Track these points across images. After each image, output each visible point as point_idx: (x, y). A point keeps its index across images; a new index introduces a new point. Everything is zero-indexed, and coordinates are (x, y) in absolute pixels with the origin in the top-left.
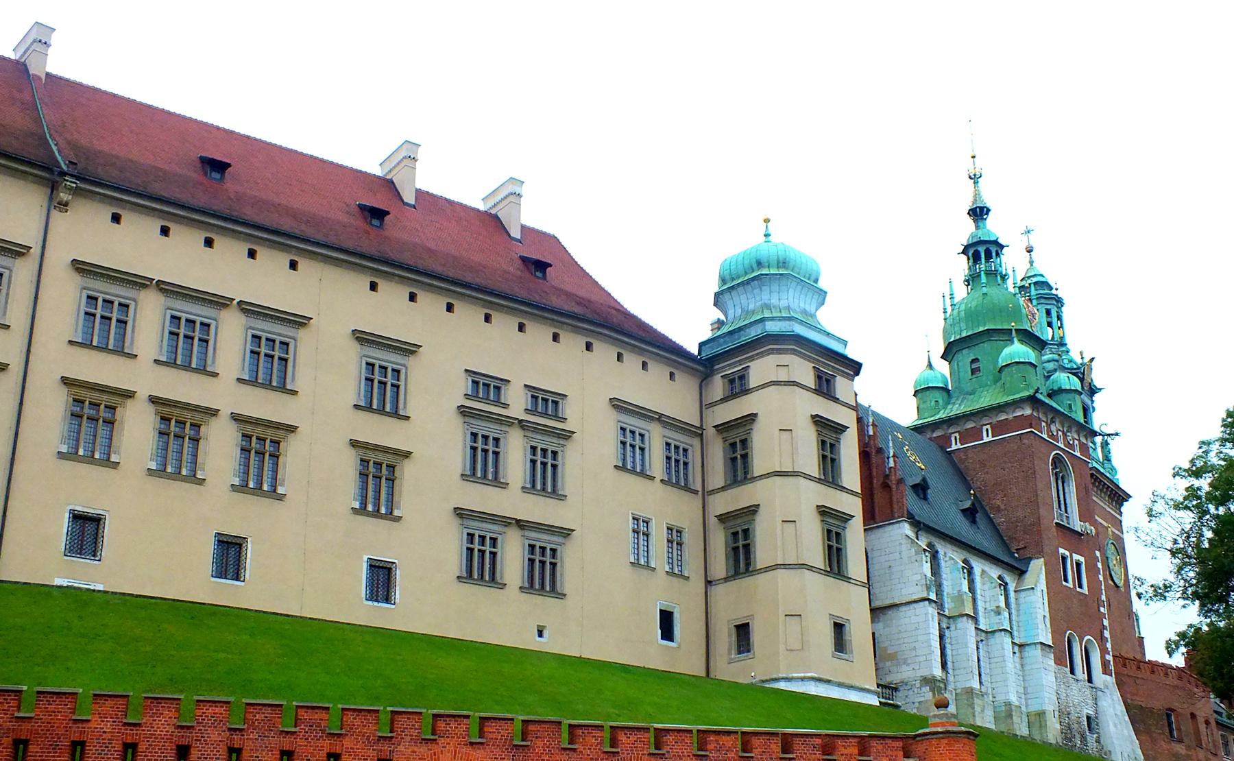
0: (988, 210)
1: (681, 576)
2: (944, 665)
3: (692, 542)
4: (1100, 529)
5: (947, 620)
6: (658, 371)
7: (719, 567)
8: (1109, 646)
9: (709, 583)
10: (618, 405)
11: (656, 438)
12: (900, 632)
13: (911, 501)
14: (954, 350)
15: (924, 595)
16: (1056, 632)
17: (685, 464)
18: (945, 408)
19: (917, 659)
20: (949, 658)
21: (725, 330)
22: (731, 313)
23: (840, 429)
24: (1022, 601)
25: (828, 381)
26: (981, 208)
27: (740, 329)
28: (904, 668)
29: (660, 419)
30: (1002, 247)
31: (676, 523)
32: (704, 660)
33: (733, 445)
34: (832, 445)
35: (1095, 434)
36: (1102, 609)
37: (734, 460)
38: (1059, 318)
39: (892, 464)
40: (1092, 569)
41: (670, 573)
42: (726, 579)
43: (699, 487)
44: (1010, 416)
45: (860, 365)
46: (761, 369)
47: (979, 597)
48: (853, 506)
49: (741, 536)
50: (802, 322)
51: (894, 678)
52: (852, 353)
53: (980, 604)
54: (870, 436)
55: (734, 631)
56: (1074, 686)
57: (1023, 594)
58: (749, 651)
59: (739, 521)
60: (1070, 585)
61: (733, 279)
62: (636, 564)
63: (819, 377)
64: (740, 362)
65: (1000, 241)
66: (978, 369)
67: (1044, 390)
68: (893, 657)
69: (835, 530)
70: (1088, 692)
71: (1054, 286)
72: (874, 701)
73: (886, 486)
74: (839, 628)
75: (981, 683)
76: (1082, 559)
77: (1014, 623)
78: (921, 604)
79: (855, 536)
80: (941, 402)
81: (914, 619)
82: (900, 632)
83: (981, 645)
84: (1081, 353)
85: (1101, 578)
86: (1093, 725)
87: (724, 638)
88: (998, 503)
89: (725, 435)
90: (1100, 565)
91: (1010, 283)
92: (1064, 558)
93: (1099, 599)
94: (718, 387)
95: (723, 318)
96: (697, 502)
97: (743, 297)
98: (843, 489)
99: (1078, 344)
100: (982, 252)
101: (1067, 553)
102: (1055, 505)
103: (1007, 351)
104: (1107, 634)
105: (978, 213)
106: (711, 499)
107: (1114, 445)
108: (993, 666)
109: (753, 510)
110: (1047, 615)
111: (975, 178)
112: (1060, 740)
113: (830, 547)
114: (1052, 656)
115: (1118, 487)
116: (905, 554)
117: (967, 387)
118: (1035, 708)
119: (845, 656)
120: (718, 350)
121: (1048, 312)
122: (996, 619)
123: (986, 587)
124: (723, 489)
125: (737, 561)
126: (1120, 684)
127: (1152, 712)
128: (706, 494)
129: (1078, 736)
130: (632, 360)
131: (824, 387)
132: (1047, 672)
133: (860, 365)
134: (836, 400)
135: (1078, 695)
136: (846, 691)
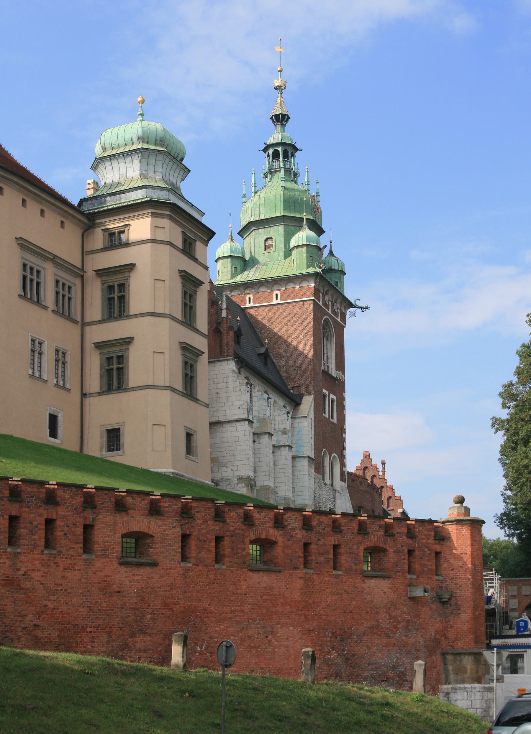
0: (289, 118)
1: (64, 388)
3: (73, 359)
6: (52, 219)
7: (94, 382)
9: (84, 395)
10: (24, 245)
11: (49, 275)
12: (223, 442)
15: (245, 416)
16: (318, 449)
17: (69, 299)
24: (296, 425)
25: (190, 244)
26: (284, 116)
28: (224, 469)
29: (54, 259)
30: (296, 150)
31: (61, 346)
34: (191, 296)
37: (111, 300)
41: (57, 385)
42: (100, 394)
43: (79, 319)
48: (201, 344)
49: (115, 360)
52: (205, 221)
57: (297, 421)
58: (118, 449)
59: (114, 349)
60: (327, 415)
61: (113, 148)
62: (33, 376)
63: (185, 240)
69: (190, 362)
74: (189, 436)
76: (335, 398)
78: (242, 423)
82: (223, 442)
88: (281, 351)
89: (104, 278)
97: (122, 165)
98: (197, 331)
106: (88, 329)
108: (278, 471)
109: (128, 341)
110: (313, 436)
113: (186, 375)
114: (313, 466)
119: (193, 458)
124: (100, 322)
128: (84, 324)
130: (34, 207)
133: (214, 234)
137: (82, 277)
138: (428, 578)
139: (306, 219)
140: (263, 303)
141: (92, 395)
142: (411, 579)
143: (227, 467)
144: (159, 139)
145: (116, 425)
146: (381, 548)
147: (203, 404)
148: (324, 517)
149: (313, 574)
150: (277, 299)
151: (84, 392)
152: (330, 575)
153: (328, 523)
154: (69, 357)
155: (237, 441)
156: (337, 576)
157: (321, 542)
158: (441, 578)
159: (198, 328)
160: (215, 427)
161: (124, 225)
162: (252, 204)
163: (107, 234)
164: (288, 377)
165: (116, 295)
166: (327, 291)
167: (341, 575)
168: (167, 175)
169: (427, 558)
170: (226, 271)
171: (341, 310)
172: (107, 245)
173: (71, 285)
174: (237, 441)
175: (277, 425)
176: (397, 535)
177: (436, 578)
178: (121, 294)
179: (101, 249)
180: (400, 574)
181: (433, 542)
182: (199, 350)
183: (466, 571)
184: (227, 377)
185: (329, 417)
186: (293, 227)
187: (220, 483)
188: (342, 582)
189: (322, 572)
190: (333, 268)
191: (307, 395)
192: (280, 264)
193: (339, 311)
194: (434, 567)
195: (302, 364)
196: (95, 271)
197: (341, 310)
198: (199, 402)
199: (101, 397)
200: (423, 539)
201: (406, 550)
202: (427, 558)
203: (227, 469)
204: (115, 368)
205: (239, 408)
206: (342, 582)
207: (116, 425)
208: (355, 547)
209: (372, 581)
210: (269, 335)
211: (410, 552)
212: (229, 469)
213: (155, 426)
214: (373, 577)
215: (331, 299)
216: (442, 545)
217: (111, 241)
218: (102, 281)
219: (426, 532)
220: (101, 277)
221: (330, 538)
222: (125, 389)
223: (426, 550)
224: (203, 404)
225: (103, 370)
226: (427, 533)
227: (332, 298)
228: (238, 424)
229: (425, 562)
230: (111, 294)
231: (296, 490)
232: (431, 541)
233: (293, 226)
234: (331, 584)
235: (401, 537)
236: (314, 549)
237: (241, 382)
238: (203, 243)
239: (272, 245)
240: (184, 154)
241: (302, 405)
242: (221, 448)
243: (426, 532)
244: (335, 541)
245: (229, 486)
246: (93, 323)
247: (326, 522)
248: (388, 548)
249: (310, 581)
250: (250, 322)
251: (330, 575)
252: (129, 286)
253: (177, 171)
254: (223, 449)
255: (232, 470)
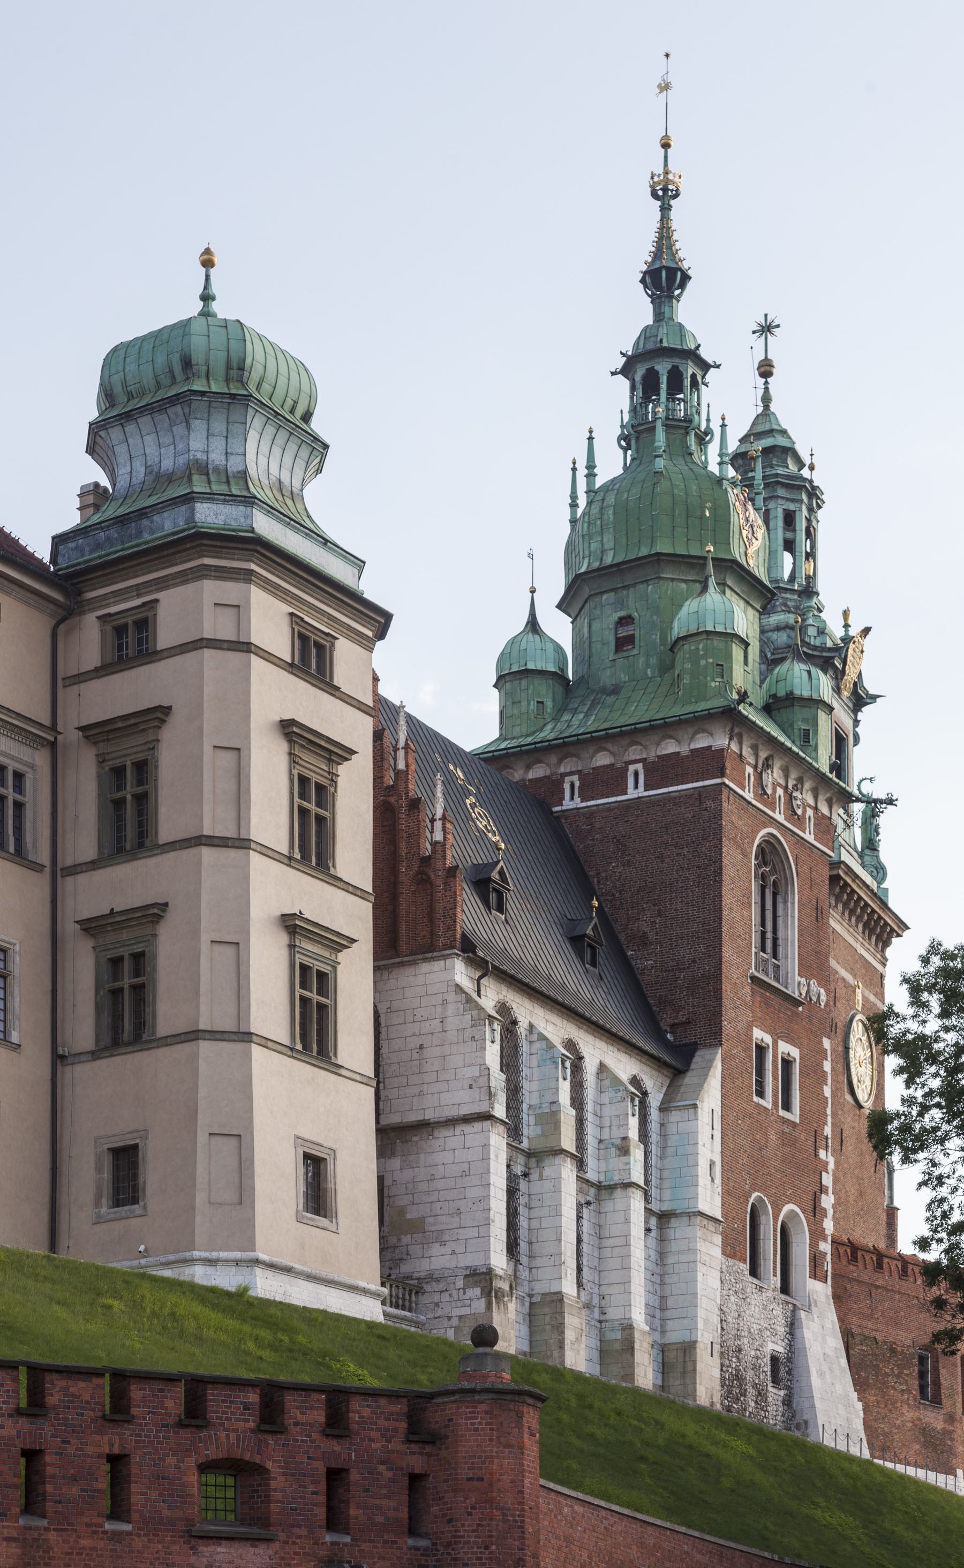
2: (512, 1248)
4: (841, 992)
5: (531, 1158)
7: (82, 1030)
8: (829, 1225)
9: (58, 1059)
12: (432, 1179)
13: (470, 913)
14: (586, 591)
18: (556, 719)
19: (463, 1234)
20: (523, 1234)
21: (110, 511)
22: (123, 472)
23: (336, 753)
24: (672, 1129)
27: (142, 513)
28: (436, 1249)
32: (45, 1215)
33: (119, 772)
35: (846, 798)
36: (822, 1154)
38: (810, 534)
39: (438, 836)
40: (813, 1073)
42: (95, 1055)
44: (684, 749)
45: (388, 617)
46: (185, 608)
47: (590, 1116)
48: (353, 917)
49: (127, 966)
50: (271, 510)
51: (419, 1266)
52: (371, 588)
53: (591, 1131)
54: (398, 773)
55: (107, 1161)
56: (756, 1300)
58: (135, 1201)
59: (125, 935)
60: (767, 1103)
64: (138, 590)
65: (704, 353)
66: (630, 640)
67: (757, 696)
68: (417, 1226)
69: (318, 966)
70: (778, 1311)
71: (807, 460)
72: (371, 1310)
73: (423, 880)
75: (580, 1285)
76: (795, 1053)
77: (653, 1171)
79: (355, 977)
80: (549, 704)
81: (461, 1155)
82: (432, 1179)
83: (586, 1212)
84: (846, 614)
85: (827, 1091)
86: (782, 1372)
87: (86, 1176)
90: (827, 1066)
91: (713, 449)
92: (761, 1050)
93: (817, 1134)
94: (89, 641)
95: (105, 482)
96: (39, 885)
98: (336, 882)
99: (841, 596)
100: (662, 370)
101: (768, 1039)
102: (755, 939)
103: (690, 606)
104: (827, 1201)
105: (664, 279)
106: (69, 884)
107: (886, 819)
109: (153, 914)
111: (664, 193)
112: (717, 1399)
114: (718, 1239)
115: (884, 905)
116: (453, 1023)
117: (607, 678)
118: (675, 1336)
120: (91, 556)
121: (789, 519)
122: (616, 1162)
123: (605, 1098)
124: (93, 865)
125: (117, 1017)
126: (838, 1298)
127: (893, 1351)
128: (59, 873)
129: (751, 1391)
131: (311, 659)
132: (709, 1265)
133: (388, 617)
134: (333, 690)
135: (762, 1312)
136: (322, 1290)
137: (53, 745)
138: (385, 1542)
139: (713, 559)
140: (603, 797)
141: (78, 1058)
142: (333, 1544)
143: (443, 1243)
144: (235, 364)
145: (129, 1136)
146: (248, 1462)
147: (358, 1077)
148: (82, 1384)
149: (46, 1529)
150: (636, 787)
151: (60, 1051)
152: (96, 1532)
153: (92, 1397)
154: (18, 959)
155: (465, 1174)
156: (116, 1537)
157: (71, 1450)
158: (423, 1543)
159: (340, 874)
160: (416, 1139)
161: (144, 604)
162: (586, 525)
163: (108, 628)
164: (661, 997)
165: (129, 791)
166: (767, 759)
167: (129, 1533)
168: (263, 461)
169: (384, 1491)
170: (516, 712)
171: (816, 809)
172: (109, 659)
173: (21, 768)
174: (465, 1174)
175: (607, 1130)
176: (294, 1430)
177: (410, 1542)
178: (140, 790)
179: (96, 669)
180: (303, 1531)
181: (404, 1448)
182: (338, 934)
183: (479, 1525)
184: (445, 1002)
185: (775, 1103)
186: (684, 586)
187: (427, 1288)
188: (131, 1551)
189: (72, 1525)
190: (797, 692)
191: (706, 1046)
192: (649, 690)
193: (810, 812)
194: (404, 1514)
195: (694, 961)
196: (80, 729)
197: (816, 809)
198: (343, 1072)
199: (98, 1063)
200: (371, 1440)
201: (322, 1471)
202: (384, 1491)
203: (443, 1250)
204: (126, 986)
205: (471, 1087)
206: (131, 1551)
207: (129, 1136)
208: (172, 1460)
209: (219, 1549)
210: (618, 884)
211: (335, 1476)
212: (447, 1249)
213: (215, 1140)
214: (221, 1538)
215: (782, 782)
216: (429, 1455)
217: (120, 648)
218: (97, 755)
219: (382, 1423)
220: (95, 743)
221: (98, 1438)
222: (146, 1042)
223: (382, 1468)
224: (358, 1077)
225: (102, 993)
226: (386, 1423)
227: (786, 777)
228: (467, 1128)
229: (378, 1502)
230: (119, 790)
231: (671, 1303)
232: (396, 1445)
233: (685, 581)
234: (101, 1556)
235: (309, 1436)
236: (50, 1465)
237: (475, 1017)
238: (360, 644)
239: (633, 636)
240: (312, 398)
241: (689, 1074)
242: (428, 1193)
243: (382, 1423)
244: (111, 1445)
245: (447, 1294)
246: (79, 869)
247: (86, 1397)
248: (269, 1465)
249: (38, 1547)
250: (574, 851)
251: (96, 1532)
252: (157, 767)
253: (292, 447)
254: (434, 1197)
255: (453, 1252)
